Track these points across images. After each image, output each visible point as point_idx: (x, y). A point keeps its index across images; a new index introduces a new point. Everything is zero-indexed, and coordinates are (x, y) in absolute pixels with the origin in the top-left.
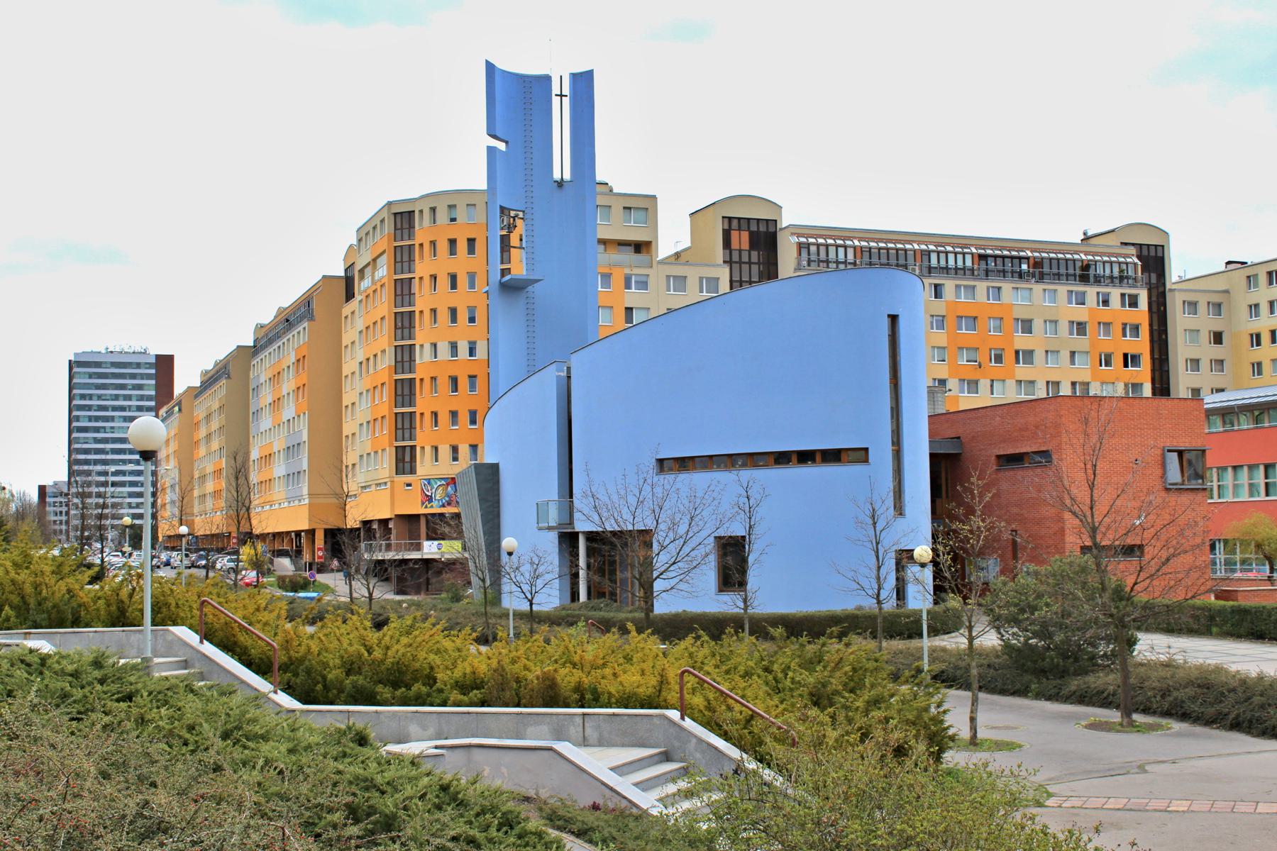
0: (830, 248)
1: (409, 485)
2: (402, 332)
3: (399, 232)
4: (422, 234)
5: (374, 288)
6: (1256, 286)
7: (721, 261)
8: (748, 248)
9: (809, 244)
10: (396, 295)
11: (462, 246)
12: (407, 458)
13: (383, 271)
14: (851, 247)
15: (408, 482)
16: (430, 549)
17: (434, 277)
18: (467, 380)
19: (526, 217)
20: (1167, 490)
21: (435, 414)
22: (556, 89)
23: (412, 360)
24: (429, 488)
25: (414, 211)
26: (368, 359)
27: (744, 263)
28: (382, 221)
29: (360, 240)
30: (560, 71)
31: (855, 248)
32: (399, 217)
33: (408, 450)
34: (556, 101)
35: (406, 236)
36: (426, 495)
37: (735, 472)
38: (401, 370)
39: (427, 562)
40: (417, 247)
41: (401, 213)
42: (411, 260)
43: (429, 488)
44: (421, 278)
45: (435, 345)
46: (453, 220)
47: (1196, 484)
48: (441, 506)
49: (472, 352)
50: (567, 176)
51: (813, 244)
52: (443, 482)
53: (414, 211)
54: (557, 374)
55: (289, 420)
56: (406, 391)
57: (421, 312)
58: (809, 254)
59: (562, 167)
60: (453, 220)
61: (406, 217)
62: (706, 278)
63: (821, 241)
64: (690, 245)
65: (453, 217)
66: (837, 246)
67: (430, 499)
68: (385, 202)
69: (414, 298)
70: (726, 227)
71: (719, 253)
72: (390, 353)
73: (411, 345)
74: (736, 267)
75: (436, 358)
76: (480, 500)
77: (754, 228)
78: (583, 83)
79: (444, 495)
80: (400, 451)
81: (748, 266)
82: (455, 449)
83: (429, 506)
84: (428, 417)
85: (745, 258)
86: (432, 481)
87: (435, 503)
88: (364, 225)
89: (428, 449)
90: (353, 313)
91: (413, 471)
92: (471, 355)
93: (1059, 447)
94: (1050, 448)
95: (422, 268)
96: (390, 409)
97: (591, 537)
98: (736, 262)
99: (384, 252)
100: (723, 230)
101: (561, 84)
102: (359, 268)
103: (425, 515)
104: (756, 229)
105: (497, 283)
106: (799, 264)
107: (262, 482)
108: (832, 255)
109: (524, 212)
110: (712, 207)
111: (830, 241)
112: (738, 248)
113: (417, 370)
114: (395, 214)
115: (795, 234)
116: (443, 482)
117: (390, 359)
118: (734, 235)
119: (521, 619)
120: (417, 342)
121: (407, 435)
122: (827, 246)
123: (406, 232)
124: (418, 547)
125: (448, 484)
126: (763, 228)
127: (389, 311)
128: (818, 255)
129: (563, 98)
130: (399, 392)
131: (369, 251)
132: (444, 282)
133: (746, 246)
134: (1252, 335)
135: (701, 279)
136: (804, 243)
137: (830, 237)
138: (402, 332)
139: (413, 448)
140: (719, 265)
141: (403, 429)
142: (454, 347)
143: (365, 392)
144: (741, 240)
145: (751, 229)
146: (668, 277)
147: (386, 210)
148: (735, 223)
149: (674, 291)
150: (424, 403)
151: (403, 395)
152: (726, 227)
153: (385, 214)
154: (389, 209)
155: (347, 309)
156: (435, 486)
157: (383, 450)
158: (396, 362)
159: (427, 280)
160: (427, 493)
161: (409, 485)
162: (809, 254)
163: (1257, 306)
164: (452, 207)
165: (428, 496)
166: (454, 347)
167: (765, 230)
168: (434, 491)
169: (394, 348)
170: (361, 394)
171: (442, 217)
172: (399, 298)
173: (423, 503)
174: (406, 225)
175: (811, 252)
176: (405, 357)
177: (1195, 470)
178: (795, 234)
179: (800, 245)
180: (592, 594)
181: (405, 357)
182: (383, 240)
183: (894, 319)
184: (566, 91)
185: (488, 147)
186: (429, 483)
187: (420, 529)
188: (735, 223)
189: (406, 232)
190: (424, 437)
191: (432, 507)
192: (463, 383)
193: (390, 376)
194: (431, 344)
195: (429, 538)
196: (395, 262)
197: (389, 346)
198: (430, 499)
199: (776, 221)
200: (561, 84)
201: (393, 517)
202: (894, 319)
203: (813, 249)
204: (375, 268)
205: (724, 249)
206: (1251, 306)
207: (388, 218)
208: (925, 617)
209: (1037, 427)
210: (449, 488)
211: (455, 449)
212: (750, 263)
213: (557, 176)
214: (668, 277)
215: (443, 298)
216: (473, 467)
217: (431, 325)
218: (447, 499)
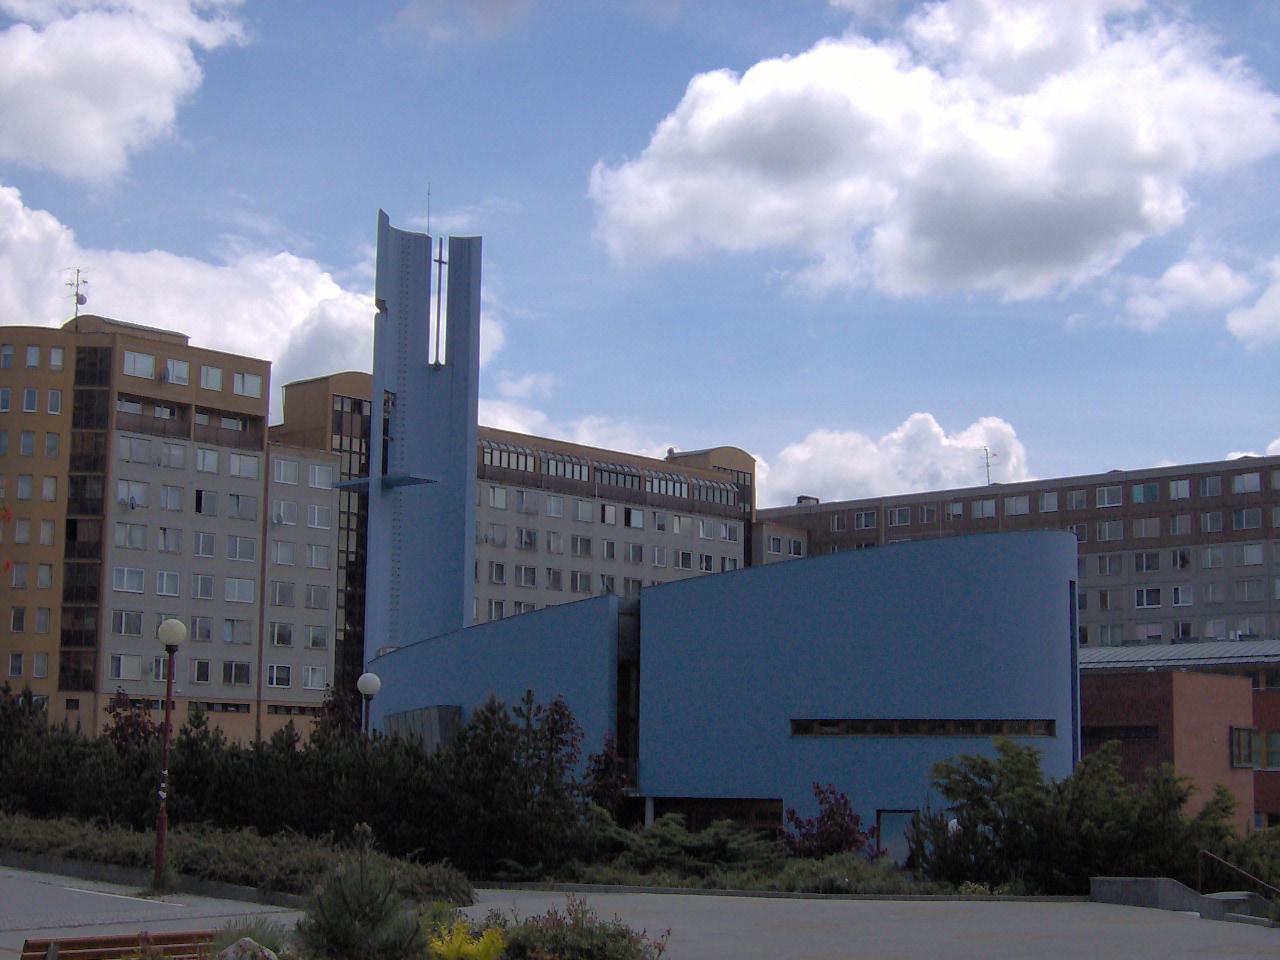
2: (349, 525)
27: (355, 452)
34: (435, 266)
50: (442, 361)
59: (437, 351)
64: (282, 422)
75: (1050, 727)
104: (340, 409)
138: (349, 525)
177: (291, 721)
180: (59, 409)
183: (802, 727)
202: (802, 727)
212: (351, 452)
213: (432, 361)
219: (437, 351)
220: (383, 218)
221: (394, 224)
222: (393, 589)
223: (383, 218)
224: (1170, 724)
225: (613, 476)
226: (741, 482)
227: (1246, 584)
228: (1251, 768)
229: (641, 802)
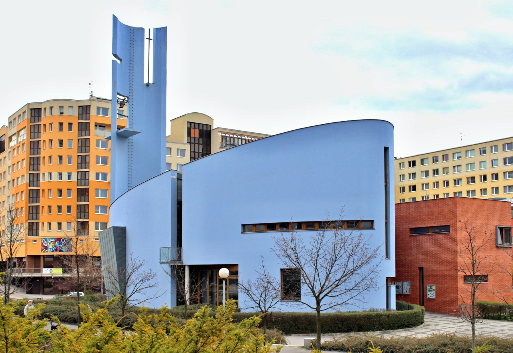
0: (235, 139)
1: (35, 241)
3: (33, 118)
4: (45, 119)
5: (18, 145)
6: (403, 167)
7: (186, 141)
8: (198, 137)
9: (226, 137)
10: (30, 149)
11: (66, 126)
12: (35, 228)
13: (24, 136)
14: (244, 139)
15: (35, 239)
16: (46, 272)
17: (51, 141)
18: (66, 191)
19: (129, 100)
20: (497, 247)
21: (50, 207)
22: (146, 35)
23: (38, 180)
24: (46, 243)
25: (41, 108)
26: (13, 180)
28: (24, 113)
29: (10, 123)
31: (246, 140)
32: (33, 111)
33: (35, 225)
34: (146, 41)
35: (36, 120)
36: (44, 246)
37: (290, 233)
38: (32, 185)
39: (41, 278)
40: (42, 126)
41: (34, 109)
42: (39, 132)
43: (46, 243)
44: (44, 141)
45: (50, 174)
46: (62, 113)
47: (506, 245)
48: (52, 252)
49: (69, 177)
50: (151, 82)
51: (228, 137)
52: (53, 240)
53: (41, 108)
54: (172, 177)
56: (35, 196)
57: (44, 157)
58: (226, 141)
59: (148, 77)
60: (62, 113)
61: (37, 111)
62: (180, 149)
63: (231, 136)
65: (62, 112)
66: (238, 139)
67: (46, 248)
68: (26, 103)
69: (40, 151)
70: (189, 127)
71: (186, 139)
72: (27, 177)
73: (38, 173)
74: (193, 145)
75: (51, 180)
76: (115, 247)
77: (201, 128)
79: (54, 246)
80: (31, 225)
81: (194, 144)
82: (60, 224)
83: (45, 251)
84: (46, 208)
85: (197, 142)
86: (48, 240)
87: (49, 250)
88: (20, 110)
89: (46, 224)
90: (5, 158)
91: (37, 234)
92: (69, 179)
93: (455, 224)
94: (450, 224)
95: (44, 136)
96: (26, 204)
97: (191, 267)
98: (193, 143)
99: (25, 128)
100: (188, 128)
101: (149, 34)
102: (9, 135)
103: (44, 256)
105: (116, 133)
106: (222, 145)
108: (236, 142)
109: (128, 97)
110: (182, 117)
111: (235, 136)
112: (194, 137)
113: (41, 185)
114: (31, 109)
115: (220, 132)
116: (53, 240)
117: (27, 179)
118: (192, 130)
119: (139, 311)
120: (41, 172)
121: (35, 217)
122: (234, 138)
123: (36, 118)
124: (39, 271)
125: (55, 241)
126: (205, 128)
127: (27, 157)
128: (230, 142)
129: (150, 40)
130: (31, 196)
131: (16, 127)
132: (56, 143)
133: (197, 136)
134: (401, 188)
135: (178, 149)
136: (224, 136)
137: (235, 134)
139: (37, 223)
140: (185, 144)
141: (33, 214)
142: (60, 174)
143: (11, 196)
144: (196, 133)
145: (200, 128)
147: (27, 106)
148: (193, 125)
150: (43, 202)
151: (33, 197)
152: (189, 127)
153: (26, 109)
154: (28, 107)
156: (49, 242)
157: (22, 224)
158: (30, 181)
159: (47, 142)
161: (35, 241)
162: (226, 141)
163: (403, 175)
164: (61, 107)
165: (45, 246)
166: (60, 174)
167: (206, 129)
168: (48, 244)
169: (29, 174)
170: (9, 197)
171: (56, 112)
172: (32, 150)
173: (42, 250)
174: (36, 115)
175: (227, 140)
176: (34, 179)
178: (220, 132)
179: (222, 136)
181: (34, 179)
182: (25, 121)
184: (152, 37)
185: (112, 60)
186: (46, 240)
187: (40, 262)
188: (193, 125)
189: (36, 118)
190: (43, 218)
191: (47, 252)
192: (65, 192)
193: (27, 188)
194: (49, 173)
195: (45, 267)
196: (31, 132)
197: (27, 173)
198: (46, 248)
199: (211, 125)
200: (149, 34)
201: (27, 256)
203: (228, 139)
204: (18, 136)
205: (188, 136)
206: (400, 176)
207: (28, 111)
209: (439, 213)
211: (60, 224)
212: (199, 144)
215: (55, 151)
216: (112, 229)
217: (49, 164)
218: (55, 248)
219: (148, 77)
223: (115, 19)
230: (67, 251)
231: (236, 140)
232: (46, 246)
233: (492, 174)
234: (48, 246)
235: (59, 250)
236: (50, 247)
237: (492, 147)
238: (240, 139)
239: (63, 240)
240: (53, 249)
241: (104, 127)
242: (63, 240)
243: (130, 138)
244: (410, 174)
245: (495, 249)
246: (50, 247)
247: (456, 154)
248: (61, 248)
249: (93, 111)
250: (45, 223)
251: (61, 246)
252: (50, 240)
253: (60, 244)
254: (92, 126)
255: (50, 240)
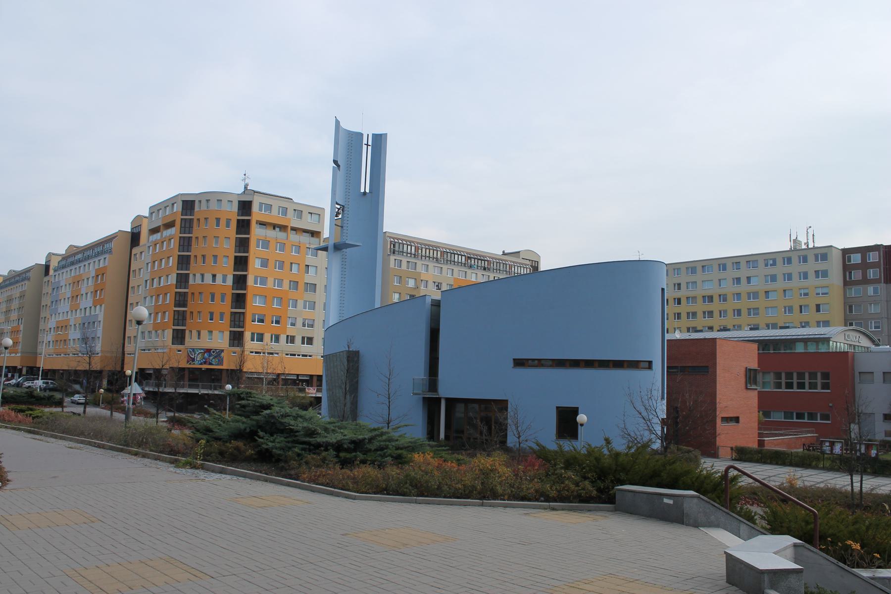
0: (404, 245)
30: (368, 131)
34: (365, 147)
45: (203, 275)
48: (200, 364)
49: (224, 281)
52: (202, 351)
55: (85, 309)
59: (365, 186)
64: (328, 236)
67: (193, 360)
75: (649, 365)
78: (379, 141)
87: (196, 362)
107: (57, 341)
121: (181, 322)
125: (205, 353)
146: (733, 263)
149: (822, 278)
155: (135, 250)
156: (197, 353)
160: (192, 356)
168: (196, 355)
173: (188, 362)
183: (519, 363)
191: (194, 364)
198: (193, 360)
202: (519, 363)
208: (40, 378)
210: (206, 355)
213: (362, 191)
214: (733, 263)
218: (204, 360)
219: (365, 186)
220: (337, 123)
221: (344, 125)
222: (341, 300)
223: (337, 123)
224: (715, 364)
225: (460, 257)
226: (534, 265)
227: (770, 309)
228: (756, 389)
229: (439, 399)
230: (218, 365)
231: (405, 246)
232: (193, 357)
233: (675, 299)
234: (195, 358)
235: (208, 363)
236: (198, 359)
237: (674, 269)
238: (428, 248)
239: (214, 352)
240: (202, 361)
241: (265, 225)
242: (214, 352)
243: (344, 250)
244: (688, 314)
245: (745, 390)
246: (198, 359)
247: (770, 309)
248: (211, 360)
249: (255, 208)
250: (193, 331)
251: (211, 358)
252: (198, 351)
253: (210, 356)
254: (253, 225)
255: (198, 351)
